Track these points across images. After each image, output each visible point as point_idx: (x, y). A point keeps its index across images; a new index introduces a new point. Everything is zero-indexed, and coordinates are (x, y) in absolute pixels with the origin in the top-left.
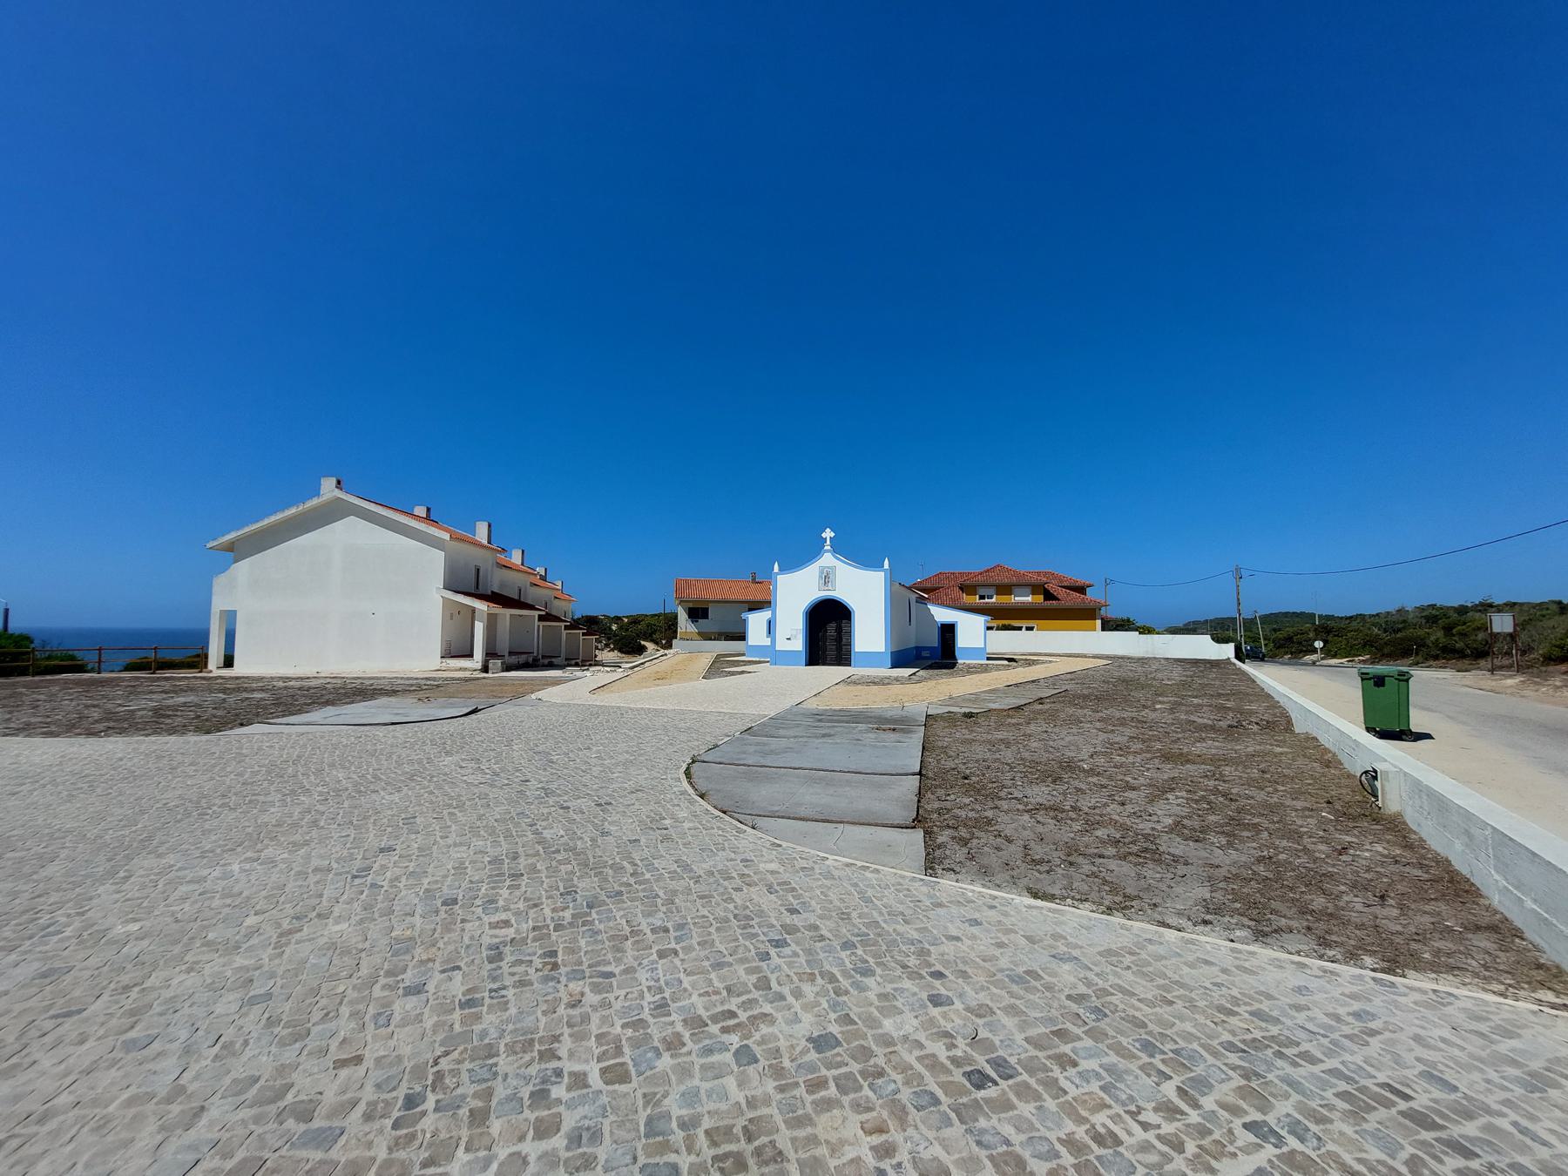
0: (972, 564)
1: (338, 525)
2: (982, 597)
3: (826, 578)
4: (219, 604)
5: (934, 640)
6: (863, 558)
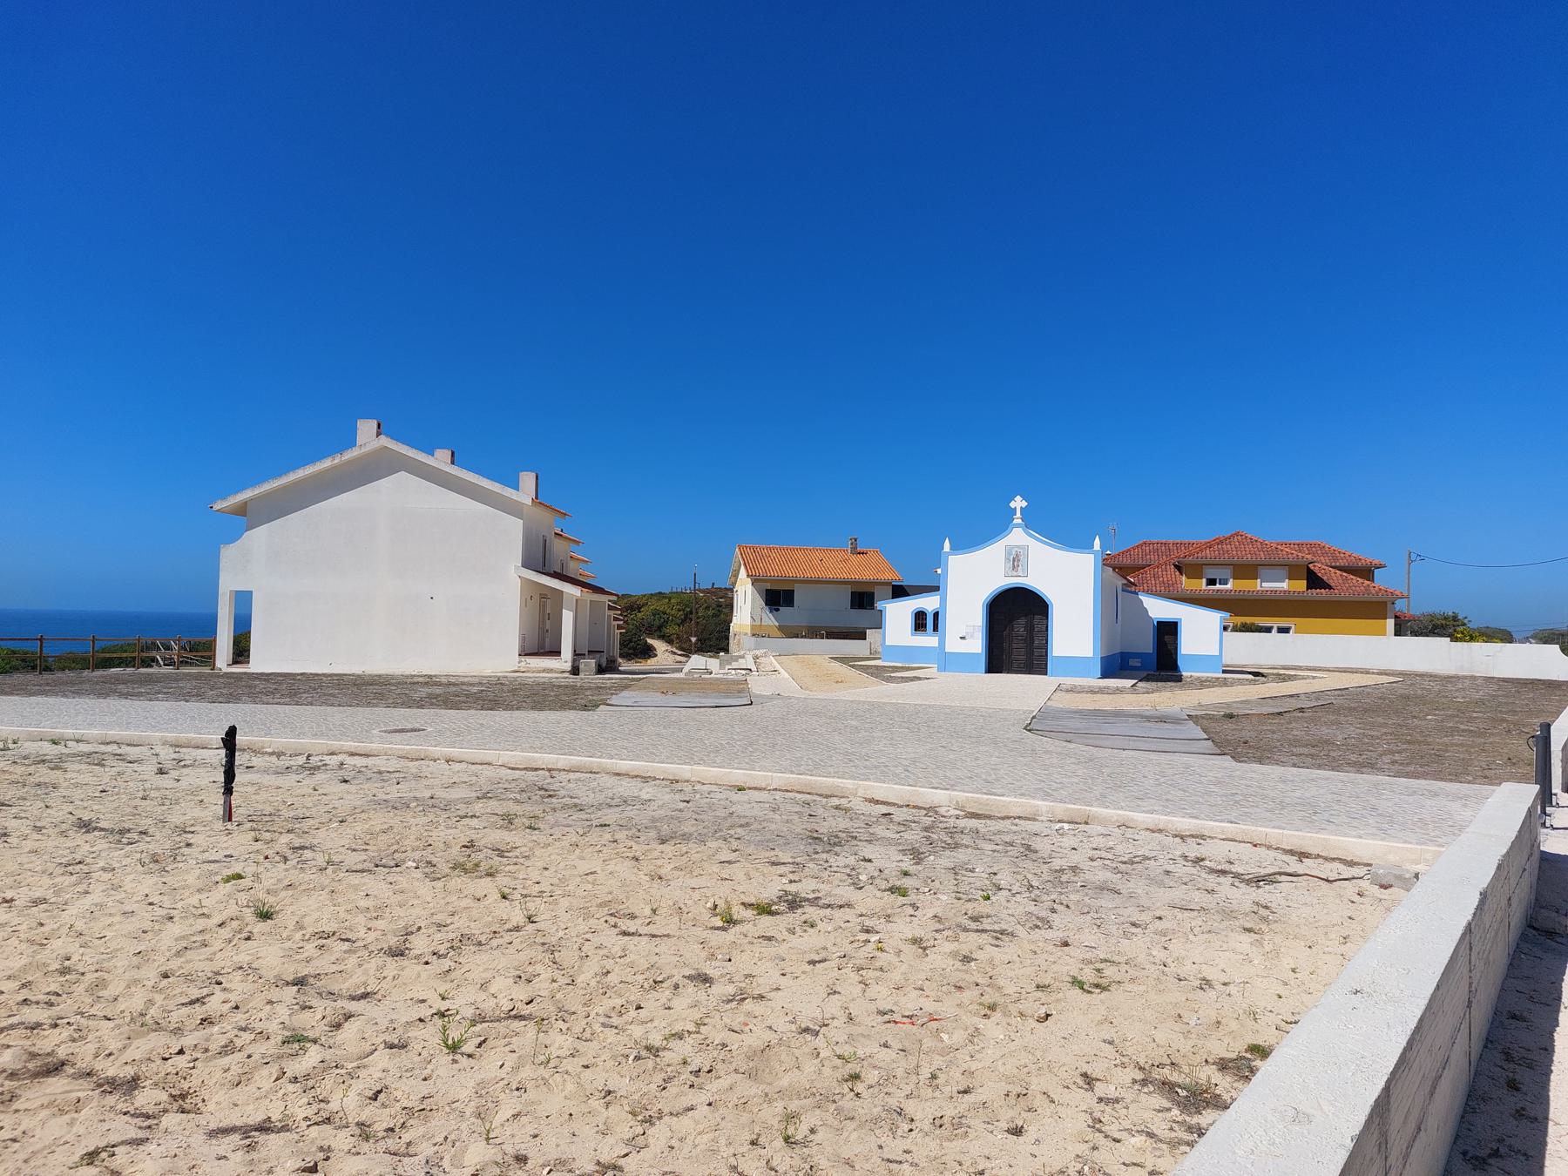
0: (1193, 528)
1: (385, 483)
2: (1212, 582)
3: (1016, 561)
4: (228, 583)
5: (1147, 645)
6: (1068, 537)
